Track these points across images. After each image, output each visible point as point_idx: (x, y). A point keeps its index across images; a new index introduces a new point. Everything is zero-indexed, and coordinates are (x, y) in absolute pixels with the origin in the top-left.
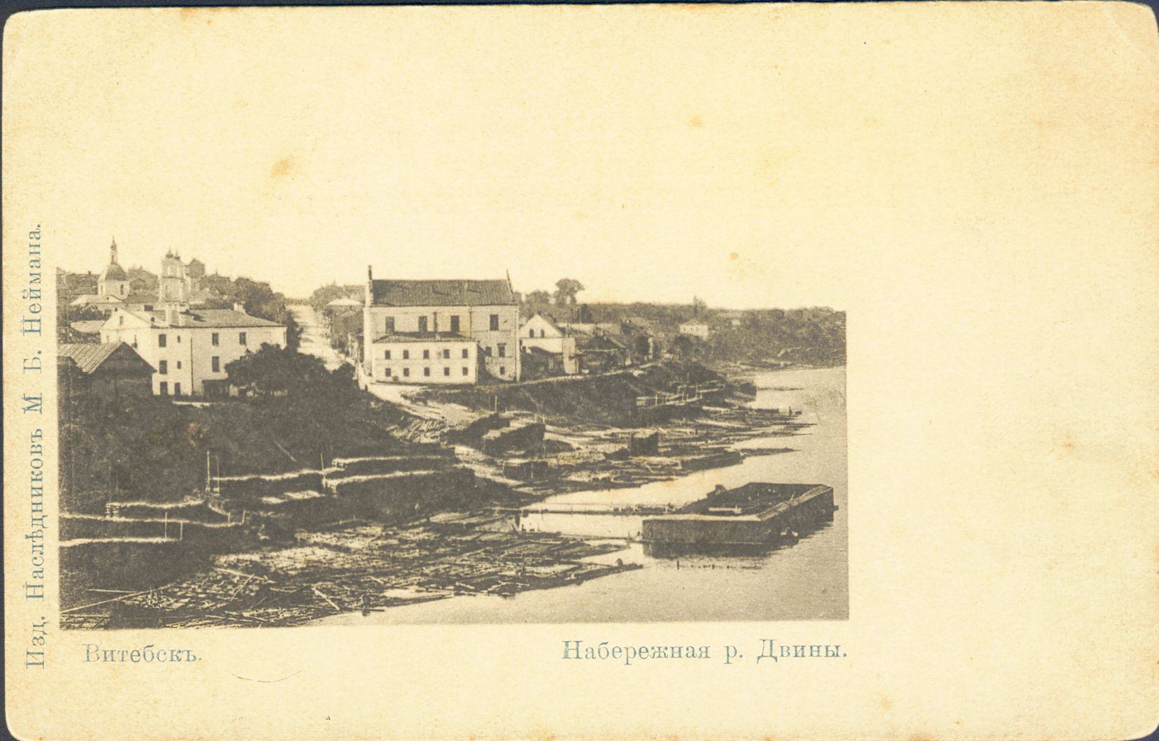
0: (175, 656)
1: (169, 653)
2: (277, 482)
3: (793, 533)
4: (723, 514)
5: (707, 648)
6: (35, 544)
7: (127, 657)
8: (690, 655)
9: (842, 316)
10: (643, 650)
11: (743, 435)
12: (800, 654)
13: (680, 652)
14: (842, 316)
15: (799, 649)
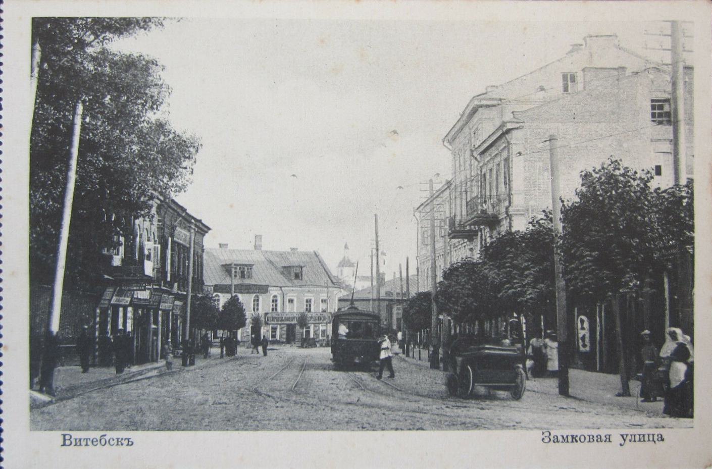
0: (119, 442)
1: (116, 441)
2: (600, 365)
3: (456, 358)
4: (601, 352)
5: (609, 436)
6: (82, 440)
7: (89, 443)
8: (556, 441)
9: (33, 19)
10: (94, 440)
11: (198, 271)
12: (642, 440)
13: (118, 442)
14: (33, 19)
15: (78, 440)
